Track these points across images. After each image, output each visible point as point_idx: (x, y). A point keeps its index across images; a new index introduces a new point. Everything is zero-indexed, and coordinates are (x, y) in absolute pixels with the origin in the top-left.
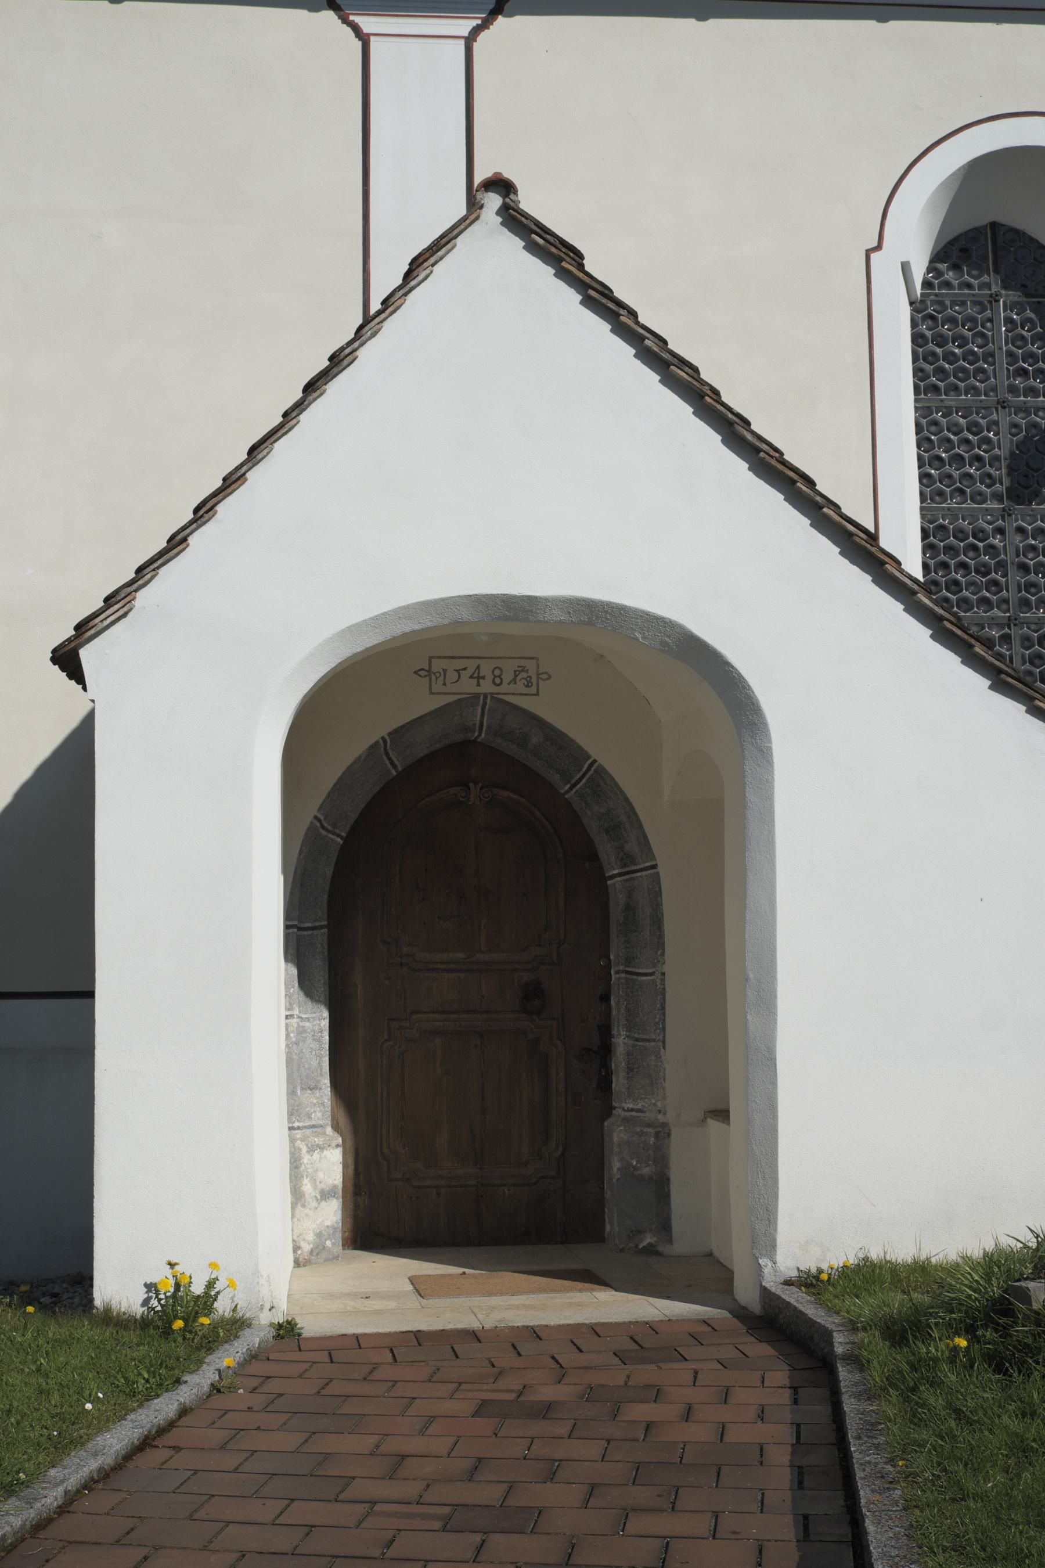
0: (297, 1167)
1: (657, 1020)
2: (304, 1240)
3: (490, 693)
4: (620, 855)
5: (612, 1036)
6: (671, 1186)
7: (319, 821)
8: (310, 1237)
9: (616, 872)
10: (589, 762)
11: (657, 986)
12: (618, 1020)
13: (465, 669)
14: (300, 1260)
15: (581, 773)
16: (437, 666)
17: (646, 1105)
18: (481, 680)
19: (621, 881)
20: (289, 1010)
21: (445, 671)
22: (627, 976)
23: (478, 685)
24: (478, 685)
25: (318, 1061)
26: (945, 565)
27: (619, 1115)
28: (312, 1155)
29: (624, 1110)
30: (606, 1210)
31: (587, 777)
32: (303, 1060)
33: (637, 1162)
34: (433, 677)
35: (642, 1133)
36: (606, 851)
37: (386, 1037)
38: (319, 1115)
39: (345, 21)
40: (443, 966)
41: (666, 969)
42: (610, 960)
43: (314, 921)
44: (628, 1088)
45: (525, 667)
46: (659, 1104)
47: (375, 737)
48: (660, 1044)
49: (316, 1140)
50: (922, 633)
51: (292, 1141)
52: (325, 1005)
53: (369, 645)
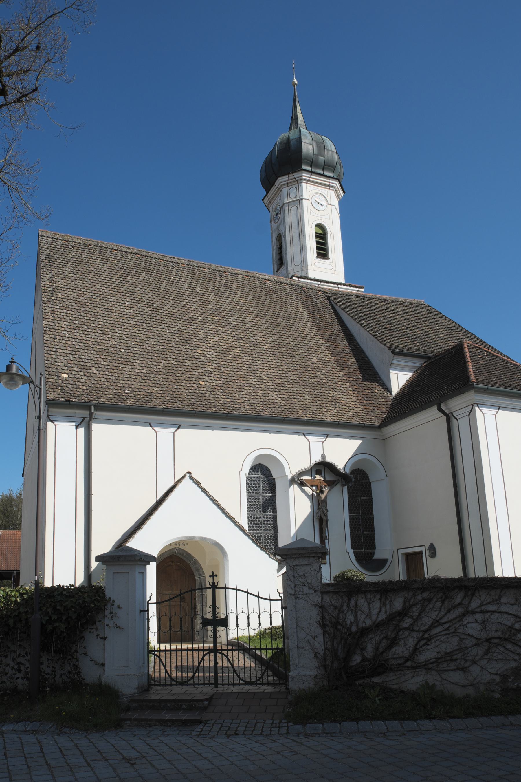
26: (251, 523)
36: (196, 574)
39: (153, 429)
50: (251, 541)
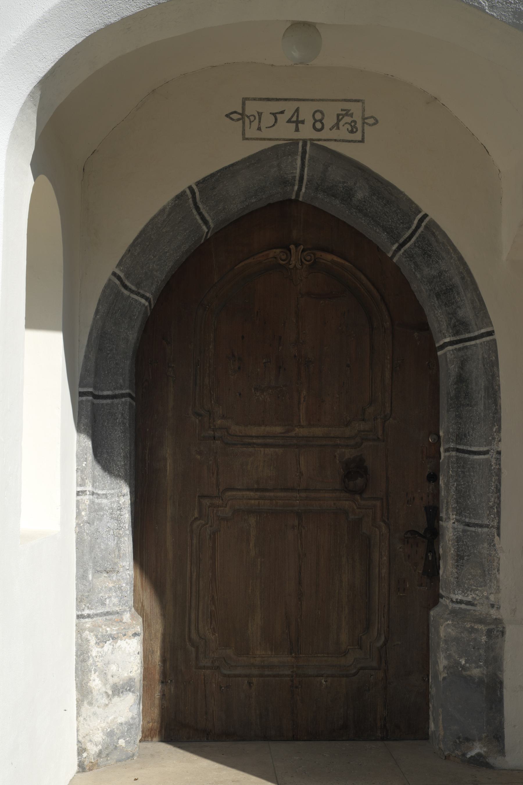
0: (84, 661)
1: (491, 504)
2: (91, 741)
3: (311, 140)
4: (453, 321)
5: (439, 519)
6: (504, 690)
7: (119, 278)
8: (99, 737)
9: (447, 340)
10: (419, 216)
11: (491, 466)
12: (447, 502)
13: (282, 112)
14: (86, 763)
15: (410, 231)
16: (251, 108)
17: (478, 598)
18: (300, 125)
19: (452, 350)
20: (81, 485)
21: (260, 114)
22: (458, 454)
23: (297, 130)
24: (297, 130)
25: (116, 542)
27: (447, 606)
28: (103, 647)
29: (452, 601)
30: (431, 705)
31: (417, 235)
32: (98, 541)
33: (466, 662)
34: (247, 121)
35: (472, 630)
37: (196, 515)
38: (115, 600)
40: (259, 441)
41: (502, 447)
42: (439, 437)
43: (115, 389)
44: (457, 578)
45: (349, 110)
46: (492, 598)
47: (181, 186)
48: (495, 531)
49: (108, 629)
51: (80, 631)
52: (126, 481)
53: (127, 13)
